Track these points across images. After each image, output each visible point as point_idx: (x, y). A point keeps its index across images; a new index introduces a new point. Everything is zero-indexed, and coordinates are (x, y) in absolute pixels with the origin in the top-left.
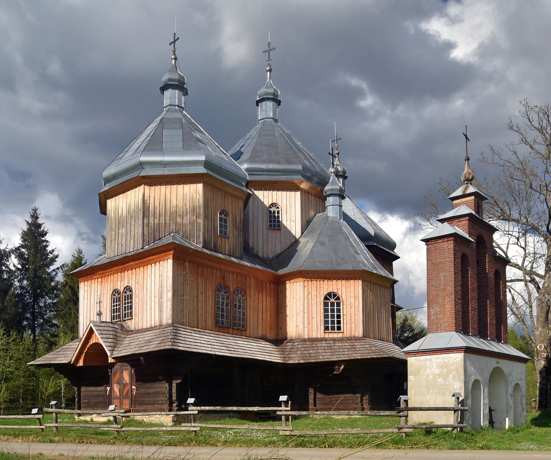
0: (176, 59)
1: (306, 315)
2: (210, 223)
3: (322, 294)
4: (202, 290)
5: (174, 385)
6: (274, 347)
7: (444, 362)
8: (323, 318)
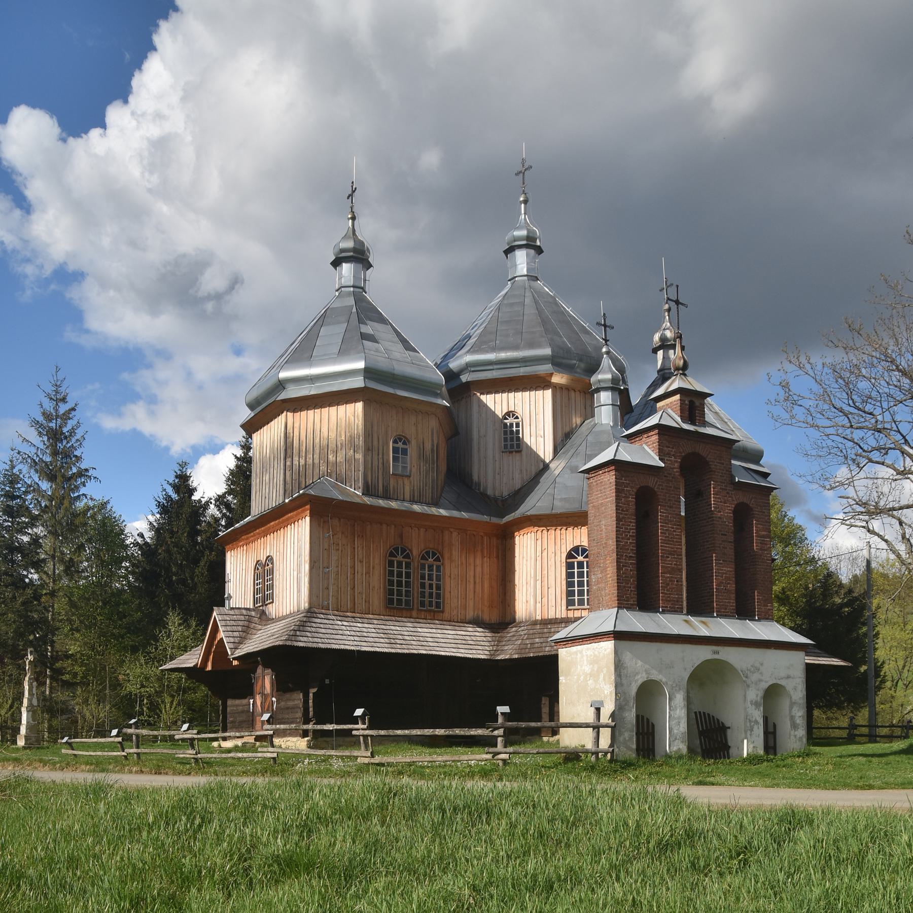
0: (353, 218)
1: (539, 583)
2: (376, 458)
3: (563, 549)
4: (361, 556)
5: (311, 695)
6: (489, 635)
7: (595, 656)
8: (564, 587)
